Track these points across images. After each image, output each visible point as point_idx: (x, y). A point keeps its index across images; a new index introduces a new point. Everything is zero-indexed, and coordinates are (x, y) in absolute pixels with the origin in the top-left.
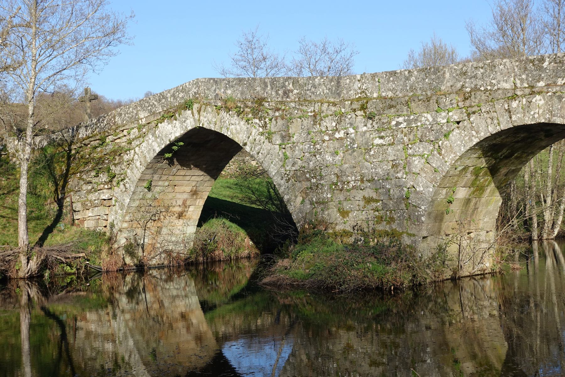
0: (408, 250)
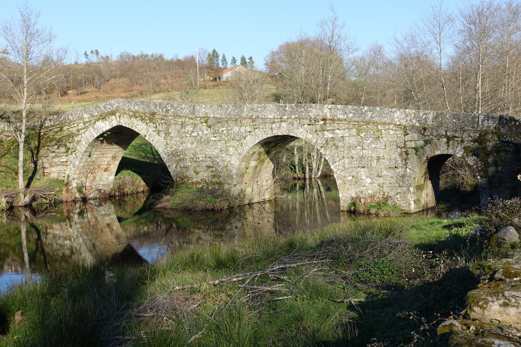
0: (227, 191)
